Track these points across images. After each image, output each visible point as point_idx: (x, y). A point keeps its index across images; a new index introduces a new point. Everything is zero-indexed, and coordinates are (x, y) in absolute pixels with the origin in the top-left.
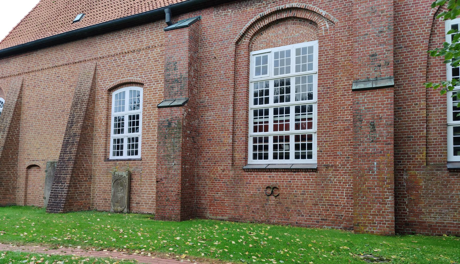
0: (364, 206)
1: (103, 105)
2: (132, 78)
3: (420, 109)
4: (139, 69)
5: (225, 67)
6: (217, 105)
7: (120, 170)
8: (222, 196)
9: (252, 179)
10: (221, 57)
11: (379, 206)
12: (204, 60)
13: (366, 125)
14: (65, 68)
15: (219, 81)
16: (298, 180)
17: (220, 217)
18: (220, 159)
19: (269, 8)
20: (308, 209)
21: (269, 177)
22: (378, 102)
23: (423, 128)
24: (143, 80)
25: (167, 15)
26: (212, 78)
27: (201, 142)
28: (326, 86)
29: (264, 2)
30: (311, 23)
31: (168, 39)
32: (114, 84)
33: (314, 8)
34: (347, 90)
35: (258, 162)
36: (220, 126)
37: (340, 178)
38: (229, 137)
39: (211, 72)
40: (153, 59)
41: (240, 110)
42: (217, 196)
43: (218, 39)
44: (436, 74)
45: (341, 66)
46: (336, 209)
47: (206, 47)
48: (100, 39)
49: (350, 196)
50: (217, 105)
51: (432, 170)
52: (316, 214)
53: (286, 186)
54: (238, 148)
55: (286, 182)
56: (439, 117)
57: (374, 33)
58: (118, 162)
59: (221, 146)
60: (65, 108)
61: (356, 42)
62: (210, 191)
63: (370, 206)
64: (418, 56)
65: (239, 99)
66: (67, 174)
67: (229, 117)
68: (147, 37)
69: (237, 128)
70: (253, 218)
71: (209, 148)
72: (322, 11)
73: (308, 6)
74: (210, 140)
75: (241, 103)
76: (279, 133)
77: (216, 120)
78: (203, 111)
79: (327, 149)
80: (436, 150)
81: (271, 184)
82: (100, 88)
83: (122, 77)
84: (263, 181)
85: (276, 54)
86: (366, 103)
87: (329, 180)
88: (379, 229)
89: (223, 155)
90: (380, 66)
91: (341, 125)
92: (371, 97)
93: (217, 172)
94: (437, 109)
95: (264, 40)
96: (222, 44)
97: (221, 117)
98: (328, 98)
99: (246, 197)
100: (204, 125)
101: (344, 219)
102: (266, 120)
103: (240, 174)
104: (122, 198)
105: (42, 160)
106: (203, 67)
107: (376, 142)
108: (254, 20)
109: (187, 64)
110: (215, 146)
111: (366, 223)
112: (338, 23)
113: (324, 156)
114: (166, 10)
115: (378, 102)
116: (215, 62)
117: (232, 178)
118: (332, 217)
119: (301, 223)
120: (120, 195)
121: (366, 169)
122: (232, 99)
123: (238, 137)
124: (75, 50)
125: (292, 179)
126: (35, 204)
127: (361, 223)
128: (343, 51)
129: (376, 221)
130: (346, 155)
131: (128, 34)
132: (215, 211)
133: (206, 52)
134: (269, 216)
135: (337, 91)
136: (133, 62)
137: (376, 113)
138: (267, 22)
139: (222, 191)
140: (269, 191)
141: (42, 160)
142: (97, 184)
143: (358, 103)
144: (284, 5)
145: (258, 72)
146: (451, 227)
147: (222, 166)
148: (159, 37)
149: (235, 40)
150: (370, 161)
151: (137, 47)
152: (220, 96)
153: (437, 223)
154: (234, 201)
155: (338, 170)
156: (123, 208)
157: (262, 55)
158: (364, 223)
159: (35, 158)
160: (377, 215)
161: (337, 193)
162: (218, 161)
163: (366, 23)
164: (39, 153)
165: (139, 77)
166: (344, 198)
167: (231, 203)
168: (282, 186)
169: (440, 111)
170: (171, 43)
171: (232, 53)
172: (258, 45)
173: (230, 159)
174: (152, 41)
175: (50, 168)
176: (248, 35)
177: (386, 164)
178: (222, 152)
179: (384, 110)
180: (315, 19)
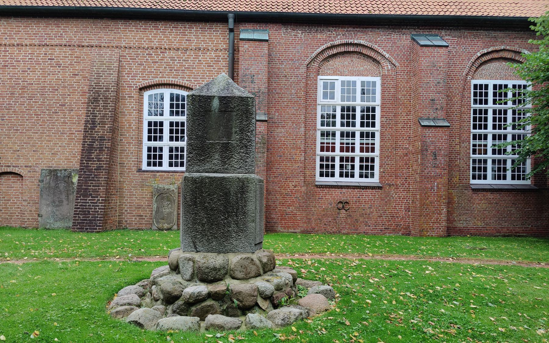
0: (427, 216)
1: (132, 106)
2: (177, 80)
3: (456, 145)
4: (186, 71)
5: (297, 87)
6: (288, 123)
7: (162, 183)
8: (294, 210)
9: (324, 195)
10: (292, 76)
11: (437, 216)
12: (273, 76)
13: (430, 154)
14: (64, 50)
15: (290, 99)
16: (366, 196)
17: (293, 230)
18: (292, 175)
19: (338, 39)
20: (374, 220)
21: (340, 193)
22: (439, 137)
23: (457, 159)
24: (192, 84)
25: (231, 21)
26: (281, 95)
27: (271, 158)
28: (389, 118)
29: (333, 32)
30: (373, 61)
31: (244, 49)
32: (149, 82)
33: (379, 49)
34: (406, 124)
35: (324, 179)
36: (291, 144)
37: (400, 194)
38: (301, 155)
39: (281, 89)
40: (206, 63)
41: (311, 130)
42: (288, 210)
43: (289, 58)
44: (464, 119)
45: (402, 103)
46: (396, 220)
47: (276, 64)
48: (124, 24)
49: (407, 209)
50: (288, 123)
51: (462, 189)
52: (380, 224)
53: (356, 201)
54: (308, 165)
55: (355, 197)
56: (465, 151)
57: (434, 83)
58: (158, 174)
59: (293, 163)
60: (67, 101)
61: (421, 87)
62: (281, 206)
63: (431, 216)
64: (455, 104)
65: (309, 119)
66: (99, 186)
67: (300, 135)
68: (197, 36)
69: (308, 147)
70: (325, 230)
71: (279, 164)
72: (386, 54)
73: (374, 46)
74: (280, 156)
75: (311, 124)
76: (365, 154)
77: (287, 137)
78: (273, 127)
79: (389, 170)
80: (463, 175)
81: (342, 199)
82: (126, 84)
83: (161, 76)
84: (335, 197)
85: (343, 83)
86: (431, 137)
87: (392, 196)
88: (436, 233)
89: (295, 171)
90: (437, 109)
91: (401, 152)
92: (434, 132)
93: (289, 188)
94: (464, 145)
95: (331, 67)
96: (293, 64)
97: (292, 135)
98: (390, 128)
99: (319, 211)
100: (274, 141)
101: (402, 228)
102: (333, 141)
103: (312, 190)
104: (170, 214)
105: (25, 166)
106: (272, 82)
107: (437, 167)
108: (324, 47)
109: (266, 79)
110: (287, 162)
111: (428, 229)
112: (399, 66)
113: (386, 176)
114: (231, 15)
115: (439, 137)
116: (285, 80)
117: (304, 194)
118: (393, 227)
119: (368, 233)
120: (166, 210)
121: (429, 188)
122: (304, 119)
123: (308, 155)
124: (82, 30)
125: (360, 195)
126: (11, 223)
127: (425, 229)
128: (403, 91)
129: (435, 227)
130: (405, 176)
131: (170, 27)
132: (286, 225)
133: (275, 68)
134: (340, 228)
135: (399, 123)
136: (177, 61)
137: (437, 145)
138: (335, 51)
139: (293, 206)
140: (340, 206)
141: (25, 166)
142: (126, 198)
143: (425, 137)
144: (353, 40)
145: (325, 96)
146: (472, 230)
147: (294, 182)
148: (214, 41)
149: (307, 62)
150: (432, 182)
151: (183, 45)
152: (291, 114)
153: (464, 227)
154: (306, 215)
155: (399, 188)
156: (171, 225)
157: (329, 81)
158: (426, 229)
159: (12, 164)
160: (435, 222)
161: (398, 207)
162: (289, 177)
163: (428, 74)
164: (18, 156)
165: (187, 80)
166: (403, 211)
167: (303, 217)
168: (352, 201)
169: (466, 147)
170: (248, 54)
171: (303, 75)
172: (326, 71)
173: (302, 176)
174: (204, 43)
175: (48, 178)
176: (317, 60)
177: (443, 184)
178: (293, 169)
179: (442, 143)
180: (379, 58)
